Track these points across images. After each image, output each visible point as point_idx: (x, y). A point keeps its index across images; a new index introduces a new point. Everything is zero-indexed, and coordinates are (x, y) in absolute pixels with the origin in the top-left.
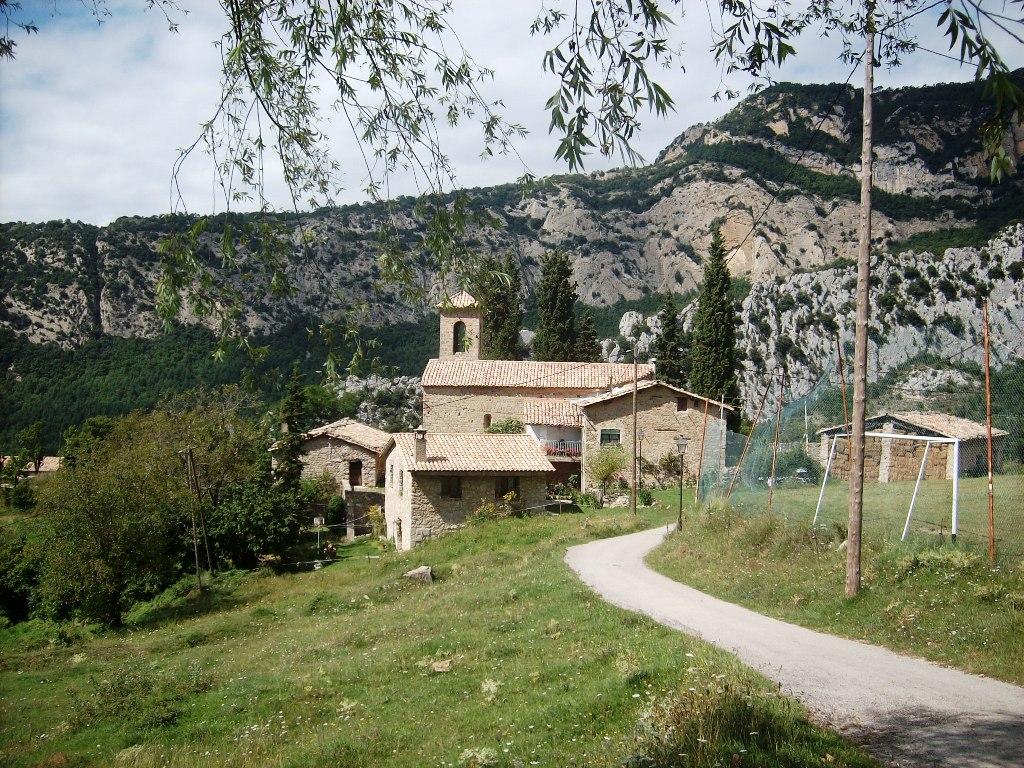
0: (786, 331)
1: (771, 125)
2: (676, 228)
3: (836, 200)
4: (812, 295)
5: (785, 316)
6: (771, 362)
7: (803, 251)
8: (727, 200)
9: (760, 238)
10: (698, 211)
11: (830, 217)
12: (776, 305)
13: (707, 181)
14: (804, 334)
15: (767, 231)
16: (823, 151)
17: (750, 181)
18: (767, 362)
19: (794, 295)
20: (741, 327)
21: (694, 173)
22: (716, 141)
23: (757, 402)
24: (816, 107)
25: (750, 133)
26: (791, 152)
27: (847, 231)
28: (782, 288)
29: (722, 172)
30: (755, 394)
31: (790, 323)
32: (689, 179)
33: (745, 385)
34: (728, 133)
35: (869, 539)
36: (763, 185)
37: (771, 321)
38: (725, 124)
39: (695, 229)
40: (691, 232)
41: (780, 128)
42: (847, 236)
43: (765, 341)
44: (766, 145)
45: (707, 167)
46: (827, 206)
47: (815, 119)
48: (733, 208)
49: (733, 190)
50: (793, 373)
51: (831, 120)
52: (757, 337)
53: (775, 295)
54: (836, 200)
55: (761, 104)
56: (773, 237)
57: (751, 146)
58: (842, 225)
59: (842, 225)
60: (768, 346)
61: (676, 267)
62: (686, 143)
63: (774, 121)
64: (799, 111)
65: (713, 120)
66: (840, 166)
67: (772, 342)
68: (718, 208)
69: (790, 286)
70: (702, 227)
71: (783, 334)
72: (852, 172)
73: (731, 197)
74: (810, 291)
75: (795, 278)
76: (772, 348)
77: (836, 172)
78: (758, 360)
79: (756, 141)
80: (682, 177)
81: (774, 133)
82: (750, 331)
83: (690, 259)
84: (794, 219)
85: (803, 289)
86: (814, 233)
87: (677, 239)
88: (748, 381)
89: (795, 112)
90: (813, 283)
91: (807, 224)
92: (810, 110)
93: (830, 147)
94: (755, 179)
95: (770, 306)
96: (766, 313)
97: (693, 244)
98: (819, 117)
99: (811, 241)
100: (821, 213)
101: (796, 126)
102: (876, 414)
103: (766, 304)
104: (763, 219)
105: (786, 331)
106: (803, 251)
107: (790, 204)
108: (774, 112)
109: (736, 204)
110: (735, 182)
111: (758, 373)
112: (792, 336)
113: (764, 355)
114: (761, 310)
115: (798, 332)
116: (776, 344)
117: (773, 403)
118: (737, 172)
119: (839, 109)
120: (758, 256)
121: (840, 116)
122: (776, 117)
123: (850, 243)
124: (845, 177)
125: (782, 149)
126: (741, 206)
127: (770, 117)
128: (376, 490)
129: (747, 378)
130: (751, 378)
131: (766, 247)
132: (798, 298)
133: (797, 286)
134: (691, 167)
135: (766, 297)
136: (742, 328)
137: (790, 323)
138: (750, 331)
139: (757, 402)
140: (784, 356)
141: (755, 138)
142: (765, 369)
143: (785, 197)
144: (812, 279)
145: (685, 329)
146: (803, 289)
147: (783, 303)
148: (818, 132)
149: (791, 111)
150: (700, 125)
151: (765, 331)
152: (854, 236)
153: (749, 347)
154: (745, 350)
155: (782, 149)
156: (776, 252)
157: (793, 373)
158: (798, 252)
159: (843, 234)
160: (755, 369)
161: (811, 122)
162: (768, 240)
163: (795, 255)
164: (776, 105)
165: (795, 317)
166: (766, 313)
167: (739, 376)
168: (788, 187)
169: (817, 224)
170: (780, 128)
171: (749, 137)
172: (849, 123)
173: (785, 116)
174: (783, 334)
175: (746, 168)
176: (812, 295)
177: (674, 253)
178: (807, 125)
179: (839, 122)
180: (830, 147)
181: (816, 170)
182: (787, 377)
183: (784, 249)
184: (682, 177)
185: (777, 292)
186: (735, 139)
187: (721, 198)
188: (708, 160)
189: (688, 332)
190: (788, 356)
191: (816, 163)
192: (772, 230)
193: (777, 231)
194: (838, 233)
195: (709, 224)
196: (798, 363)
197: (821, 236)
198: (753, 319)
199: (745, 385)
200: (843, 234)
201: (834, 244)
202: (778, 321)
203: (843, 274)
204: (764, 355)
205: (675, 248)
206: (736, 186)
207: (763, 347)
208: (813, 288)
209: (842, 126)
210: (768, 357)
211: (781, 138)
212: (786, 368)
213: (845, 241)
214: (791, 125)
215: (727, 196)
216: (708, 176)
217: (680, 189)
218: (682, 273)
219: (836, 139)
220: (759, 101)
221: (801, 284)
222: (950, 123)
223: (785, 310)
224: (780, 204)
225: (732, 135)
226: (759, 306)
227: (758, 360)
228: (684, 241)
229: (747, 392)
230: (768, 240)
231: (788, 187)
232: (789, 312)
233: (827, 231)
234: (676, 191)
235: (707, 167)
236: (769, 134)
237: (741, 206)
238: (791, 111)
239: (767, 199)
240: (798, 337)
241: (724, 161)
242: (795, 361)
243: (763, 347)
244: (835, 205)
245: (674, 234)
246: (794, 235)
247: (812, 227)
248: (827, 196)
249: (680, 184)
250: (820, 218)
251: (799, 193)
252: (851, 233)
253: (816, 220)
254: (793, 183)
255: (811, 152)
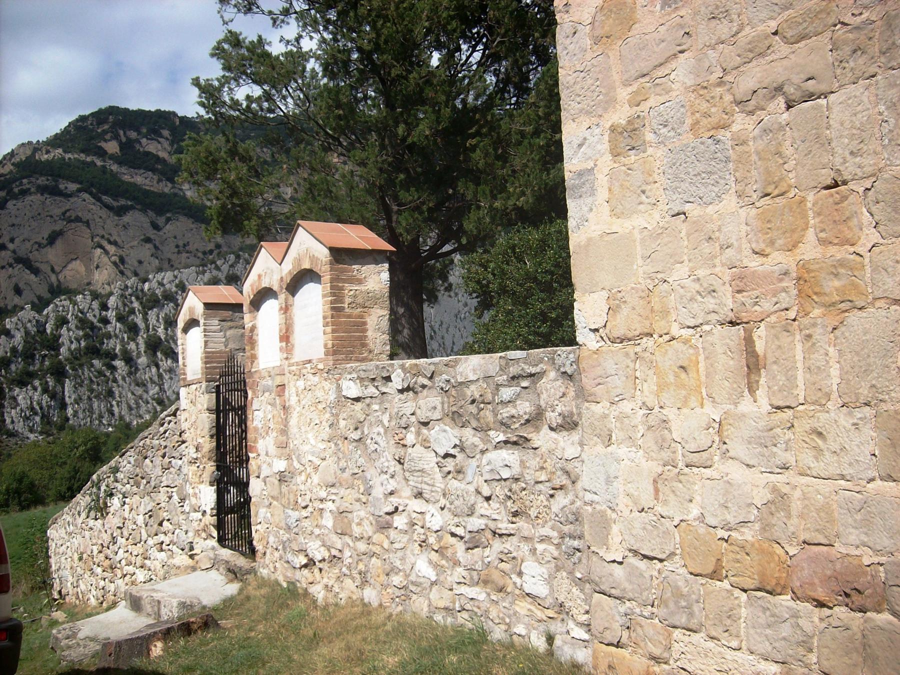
0: (154, 329)
1: (103, 144)
2: (12, 240)
3: (168, 215)
4: (176, 293)
5: (152, 314)
6: (143, 360)
7: (140, 262)
8: (64, 214)
9: (99, 251)
10: (34, 224)
11: (164, 230)
12: (141, 303)
13: (42, 194)
14: (173, 331)
15: (105, 243)
16: (154, 170)
17: (86, 196)
18: (140, 361)
19: (158, 292)
20: (109, 326)
21: (28, 186)
22: (49, 157)
23: (132, 403)
24: (145, 131)
25: (83, 151)
26: (123, 170)
27: (181, 243)
28: (146, 286)
29: (57, 186)
30: (130, 395)
31: (158, 321)
32: (24, 193)
33: (119, 386)
34: (60, 151)
35: (510, 538)
36: (99, 200)
37: (139, 320)
38: (56, 141)
39: (32, 242)
40: (28, 245)
41: (112, 147)
42: (181, 249)
43: (134, 340)
44: (99, 163)
45: (42, 181)
46: (161, 221)
47: (144, 141)
48: (70, 221)
49: (69, 203)
50: (164, 371)
51: (159, 142)
52: (126, 336)
53: (140, 293)
54: (168, 215)
55: (91, 124)
56: (112, 249)
57: (84, 162)
58: (175, 237)
59: (175, 237)
60: (137, 344)
61: (14, 280)
62: (16, 160)
63: (106, 141)
64: (128, 133)
65: (42, 138)
66: (170, 185)
67: (140, 340)
68: (55, 221)
69: (154, 284)
70: (39, 239)
71: (151, 332)
72: (181, 190)
73: (68, 210)
74: (174, 289)
75: (159, 276)
76: (142, 348)
77: (166, 190)
78: (129, 360)
79: (89, 159)
80: (16, 190)
81: (105, 153)
82: (118, 330)
83: (28, 272)
84: (131, 232)
85: (168, 286)
86: (148, 246)
87: (14, 252)
88: (121, 382)
89: (125, 133)
90: (177, 281)
91: (142, 237)
92: (139, 133)
93: (159, 167)
94: (91, 194)
95: (136, 305)
96: (132, 311)
97: (31, 256)
98: (148, 139)
99: (148, 253)
100: (156, 227)
101: (127, 146)
102: (528, 354)
103: (132, 302)
104: (101, 232)
105: (154, 329)
106: (140, 262)
107: (127, 218)
108: (105, 132)
109: (73, 218)
110: (70, 196)
111: (130, 373)
112: (161, 332)
113: (134, 354)
114: (127, 309)
115: (166, 329)
116: (146, 343)
117: (148, 403)
118: (73, 187)
119: (166, 133)
120: (98, 267)
121: (167, 139)
122: (108, 137)
123: (184, 255)
124: (175, 195)
125: (115, 168)
126: (78, 219)
127: (102, 136)
128: (477, 514)
129: (119, 378)
130: (124, 379)
131: (105, 259)
132: (163, 296)
133: (161, 284)
134: (25, 181)
135: (131, 295)
136: (110, 328)
137: (158, 321)
138: (118, 330)
139: (132, 403)
140: (155, 354)
141: (88, 155)
142: (137, 369)
143: (120, 212)
144: (176, 277)
145: (49, 331)
146: (168, 286)
147: (148, 301)
148: (148, 154)
149: (121, 132)
150: (30, 143)
151: (133, 330)
152: (187, 248)
153: (118, 348)
154: (114, 350)
155: (115, 168)
156: (115, 263)
157: (164, 371)
158: (136, 264)
159: (177, 246)
160: (126, 368)
161: (140, 143)
162: (106, 252)
163: (132, 266)
164: (106, 127)
165: (162, 315)
166: (132, 311)
167: (111, 377)
168: (123, 202)
169: (152, 237)
170: (112, 147)
171: (82, 155)
172: (175, 146)
173: (116, 137)
174: (151, 332)
175: (80, 183)
176: (176, 293)
177: (11, 265)
178: (138, 147)
179: (166, 144)
180: (159, 167)
181: (147, 188)
182: (160, 376)
183: (122, 260)
184: (16, 190)
185: (142, 290)
186: (67, 156)
187: (57, 211)
188: (41, 175)
189: (52, 333)
190: (159, 354)
191: (147, 182)
192: (110, 242)
193: (115, 243)
194: (172, 245)
195: (46, 236)
196: (169, 361)
197: (156, 248)
198: (120, 318)
199: (119, 386)
200: (177, 246)
201: (169, 255)
202: (146, 320)
203: (204, 272)
204: (134, 354)
205: (11, 261)
206: (72, 200)
207: (132, 346)
208: (177, 286)
209: (169, 149)
210: (139, 355)
211: (112, 157)
212: (157, 366)
213: (179, 252)
214: (122, 146)
215: (63, 210)
216: (43, 190)
217: (14, 202)
218: (21, 285)
219: (164, 160)
220: (89, 122)
221: (165, 282)
222: (265, 150)
223: (151, 308)
224: (116, 218)
225: (65, 152)
226: (125, 305)
227: (129, 360)
228: (22, 253)
229: (120, 394)
230: (106, 252)
231: (123, 202)
232: (155, 310)
233: (162, 243)
234: (10, 204)
235: (42, 181)
236: (102, 153)
237: (78, 219)
238: (121, 132)
239: (104, 213)
240: (167, 334)
241: (59, 176)
242: (166, 359)
243: (132, 346)
244: (168, 220)
245: (11, 246)
246: (131, 247)
247: (148, 240)
248: (160, 212)
249: (15, 197)
250: (155, 232)
251: (135, 208)
252: (185, 245)
253: (151, 233)
254: (127, 199)
255: (143, 171)
